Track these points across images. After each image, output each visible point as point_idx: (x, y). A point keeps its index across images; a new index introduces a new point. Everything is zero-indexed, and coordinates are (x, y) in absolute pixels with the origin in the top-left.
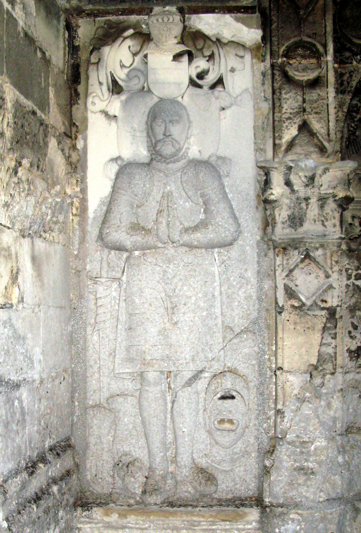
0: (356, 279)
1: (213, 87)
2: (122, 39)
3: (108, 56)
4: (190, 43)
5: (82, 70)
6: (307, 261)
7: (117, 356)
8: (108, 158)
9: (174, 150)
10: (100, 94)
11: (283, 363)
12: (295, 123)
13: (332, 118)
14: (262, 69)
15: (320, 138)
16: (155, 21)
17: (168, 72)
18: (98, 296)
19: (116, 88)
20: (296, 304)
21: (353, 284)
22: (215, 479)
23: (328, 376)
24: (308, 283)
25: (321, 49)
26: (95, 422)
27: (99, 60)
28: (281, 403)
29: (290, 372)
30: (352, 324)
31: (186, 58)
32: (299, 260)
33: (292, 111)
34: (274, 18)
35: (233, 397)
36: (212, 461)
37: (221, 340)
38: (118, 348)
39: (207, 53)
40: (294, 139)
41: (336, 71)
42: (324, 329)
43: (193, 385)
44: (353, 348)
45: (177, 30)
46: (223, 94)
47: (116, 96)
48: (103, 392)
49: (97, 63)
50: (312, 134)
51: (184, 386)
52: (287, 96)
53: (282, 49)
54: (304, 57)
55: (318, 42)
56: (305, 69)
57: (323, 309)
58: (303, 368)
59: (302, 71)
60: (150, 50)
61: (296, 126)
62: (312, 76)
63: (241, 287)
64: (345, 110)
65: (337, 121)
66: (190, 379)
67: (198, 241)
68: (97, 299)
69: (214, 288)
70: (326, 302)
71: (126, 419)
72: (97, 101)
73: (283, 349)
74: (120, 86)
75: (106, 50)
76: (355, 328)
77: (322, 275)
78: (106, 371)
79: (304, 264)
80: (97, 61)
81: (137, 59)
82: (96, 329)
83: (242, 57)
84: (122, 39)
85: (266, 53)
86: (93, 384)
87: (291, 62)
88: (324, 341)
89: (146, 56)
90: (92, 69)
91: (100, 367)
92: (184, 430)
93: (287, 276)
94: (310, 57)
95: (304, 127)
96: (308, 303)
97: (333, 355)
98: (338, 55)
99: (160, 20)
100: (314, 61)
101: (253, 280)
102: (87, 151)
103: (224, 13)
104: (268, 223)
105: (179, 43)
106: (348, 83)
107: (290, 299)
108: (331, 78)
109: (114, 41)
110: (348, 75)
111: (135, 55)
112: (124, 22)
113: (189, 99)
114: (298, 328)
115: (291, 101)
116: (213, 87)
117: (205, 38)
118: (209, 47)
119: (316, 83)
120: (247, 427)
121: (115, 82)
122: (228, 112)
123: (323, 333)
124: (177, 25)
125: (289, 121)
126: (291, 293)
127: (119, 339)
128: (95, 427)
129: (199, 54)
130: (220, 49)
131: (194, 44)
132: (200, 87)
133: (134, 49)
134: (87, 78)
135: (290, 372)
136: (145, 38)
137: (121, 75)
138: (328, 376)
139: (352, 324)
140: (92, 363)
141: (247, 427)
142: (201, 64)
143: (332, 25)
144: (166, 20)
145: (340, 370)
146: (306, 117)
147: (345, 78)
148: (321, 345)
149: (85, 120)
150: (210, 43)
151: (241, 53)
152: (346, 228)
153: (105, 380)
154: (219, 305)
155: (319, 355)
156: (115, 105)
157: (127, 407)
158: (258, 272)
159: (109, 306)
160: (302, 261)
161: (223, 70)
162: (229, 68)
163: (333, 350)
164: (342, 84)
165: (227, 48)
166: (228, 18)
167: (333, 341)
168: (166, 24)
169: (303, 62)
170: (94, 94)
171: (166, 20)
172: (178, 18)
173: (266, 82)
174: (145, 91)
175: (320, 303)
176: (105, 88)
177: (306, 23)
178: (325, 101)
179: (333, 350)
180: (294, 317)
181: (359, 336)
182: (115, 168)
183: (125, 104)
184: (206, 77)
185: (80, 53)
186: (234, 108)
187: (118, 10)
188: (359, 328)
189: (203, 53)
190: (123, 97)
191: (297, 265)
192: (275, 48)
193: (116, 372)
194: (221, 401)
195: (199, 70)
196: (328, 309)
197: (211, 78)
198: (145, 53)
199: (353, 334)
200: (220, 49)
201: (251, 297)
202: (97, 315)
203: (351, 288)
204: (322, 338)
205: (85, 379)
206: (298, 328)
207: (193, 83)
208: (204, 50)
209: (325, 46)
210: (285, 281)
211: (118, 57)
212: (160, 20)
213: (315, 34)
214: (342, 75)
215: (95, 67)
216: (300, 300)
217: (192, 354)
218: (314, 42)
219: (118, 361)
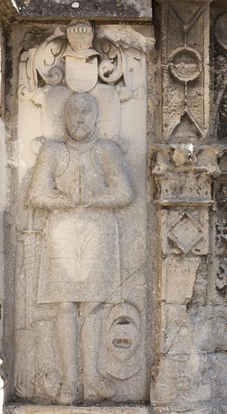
0: (224, 234)
1: (116, 83)
2: (46, 43)
3: (34, 58)
4: (99, 48)
5: (14, 66)
6: (185, 220)
7: (39, 291)
8: (35, 137)
9: (85, 133)
10: (27, 85)
11: (166, 297)
12: (178, 114)
13: (207, 110)
14: (155, 70)
15: (197, 126)
16: (72, 31)
17: (82, 71)
18: (25, 244)
19: (41, 82)
20: (177, 253)
21: (222, 237)
22: (4, 212)
23: (201, 307)
24: (187, 234)
25: (200, 58)
26: (22, 341)
27: (28, 59)
28: (164, 327)
29: (171, 304)
30: (221, 268)
31: (95, 60)
32: (179, 219)
33: (176, 104)
34: (164, 32)
35: (128, 323)
36: (111, 372)
37: (119, 279)
38: (40, 284)
39: (113, 56)
40: (177, 126)
41: (211, 72)
42: (198, 272)
43: (98, 313)
44: (221, 287)
45: (89, 38)
46: (124, 89)
47: (40, 89)
48: (28, 319)
49: (26, 61)
50: (191, 123)
51: (90, 314)
52: (173, 93)
53: (171, 55)
54: (186, 62)
55: (198, 50)
56: (188, 71)
57: (197, 256)
58: (181, 300)
59: (185, 72)
60: (68, 52)
61: (180, 116)
62: (192, 78)
63: (135, 238)
64: (218, 103)
65: (211, 111)
66: (95, 309)
67: (103, 203)
68: (24, 246)
69: (115, 240)
70: (199, 251)
71: (45, 339)
72: (25, 91)
73: (166, 286)
74: (44, 81)
75: (32, 51)
76: (222, 271)
77: (197, 231)
78: (31, 303)
79: (183, 222)
80: (26, 59)
81: (57, 58)
82: (23, 269)
83: (139, 60)
84: (46, 43)
85: (157, 57)
86: (20, 313)
87: (176, 66)
88: (198, 281)
89: (64, 58)
90: (22, 66)
91: (25, 299)
92: (90, 347)
93: (170, 231)
94: (191, 63)
95: (185, 118)
96: (186, 252)
97: (204, 291)
98: (213, 59)
99: (76, 30)
100: (194, 65)
101: (144, 234)
102: (3, 90)
103: (126, 24)
104: (156, 192)
105: (90, 48)
106: (221, 82)
107: (172, 248)
108: (207, 79)
109: (39, 45)
110: (220, 75)
111: (55, 56)
112: (47, 29)
113: (100, 91)
114: (177, 270)
115: (175, 97)
116: (116, 83)
117: (110, 42)
118: (114, 51)
119: (194, 83)
120: (138, 346)
121: (39, 77)
122: (128, 104)
123: (197, 274)
124: (89, 34)
125: (174, 113)
126: (172, 243)
127: (41, 278)
128: (21, 345)
129: (106, 56)
130: (122, 54)
131: (101, 49)
132: (106, 83)
133: (55, 52)
134: (18, 73)
135: (171, 304)
136: (64, 42)
137: (44, 71)
138: (201, 307)
139: (221, 268)
140: (20, 295)
141: (138, 346)
142: (107, 65)
143: (209, 38)
144: (81, 30)
145: (210, 303)
146: (187, 110)
147: (218, 78)
148: (195, 283)
149: (16, 106)
150: (115, 48)
151: (138, 57)
152: (216, 194)
153: (30, 309)
154: (118, 253)
155: (194, 291)
156: (40, 96)
157: (45, 328)
158: (148, 227)
159: (34, 251)
160: (182, 219)
161: (124, 71)
162: (129, 69)
163: (205, 288)
164: (215, 83)
165: (128, 53)
166: (129, 28)
167: (205, 281)
168: (81, 36)
169: (186, 66)
170: (22, 87)
171: (81, 30)
172: (89, 29)
173: (157, 80)
174: (63, 84)
175: (194, 252)
176: (32, 82)
177: (189, 36)
178: (202, 98)
179: (205, 288)
180: (174, 261)
181: (226, 278)
182: (39, 145)
183: (48, 95)
184: (110, 75)
185: (12, 52)
186: (132, 100)
187: (43, 21)
188: (226, 271)
189: (108, 56)
190: (47, 89)
191: (178, 223)
192: (164, 55)
193: (38, 303)
194: (119, 325)
195: (106, 71)
196: (201, 256)
197: (115, 77)
198: (64, 55)
199: (220, 276)
200: (122, 54)
201: (142, 246)
202: (24, 258)
203: (220, 241)
204: (196, 278)
205: (14, 310)
206: (177, 270)
207: (100, 80)
208: (110, 54)
209: (202, 54)
210: (168, 235)
211: (42, 57)
212: (76, 30)
213: (196, 44)
214: (216, 76)
215: (24, 64)
216: (179, 249)
217: (97, 289)
218: (195, 51)
219: (40, 294)
